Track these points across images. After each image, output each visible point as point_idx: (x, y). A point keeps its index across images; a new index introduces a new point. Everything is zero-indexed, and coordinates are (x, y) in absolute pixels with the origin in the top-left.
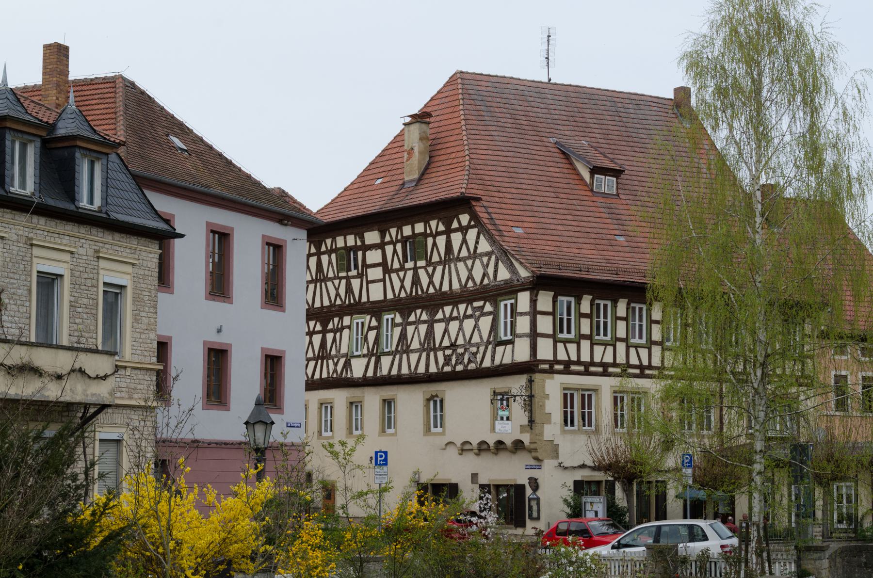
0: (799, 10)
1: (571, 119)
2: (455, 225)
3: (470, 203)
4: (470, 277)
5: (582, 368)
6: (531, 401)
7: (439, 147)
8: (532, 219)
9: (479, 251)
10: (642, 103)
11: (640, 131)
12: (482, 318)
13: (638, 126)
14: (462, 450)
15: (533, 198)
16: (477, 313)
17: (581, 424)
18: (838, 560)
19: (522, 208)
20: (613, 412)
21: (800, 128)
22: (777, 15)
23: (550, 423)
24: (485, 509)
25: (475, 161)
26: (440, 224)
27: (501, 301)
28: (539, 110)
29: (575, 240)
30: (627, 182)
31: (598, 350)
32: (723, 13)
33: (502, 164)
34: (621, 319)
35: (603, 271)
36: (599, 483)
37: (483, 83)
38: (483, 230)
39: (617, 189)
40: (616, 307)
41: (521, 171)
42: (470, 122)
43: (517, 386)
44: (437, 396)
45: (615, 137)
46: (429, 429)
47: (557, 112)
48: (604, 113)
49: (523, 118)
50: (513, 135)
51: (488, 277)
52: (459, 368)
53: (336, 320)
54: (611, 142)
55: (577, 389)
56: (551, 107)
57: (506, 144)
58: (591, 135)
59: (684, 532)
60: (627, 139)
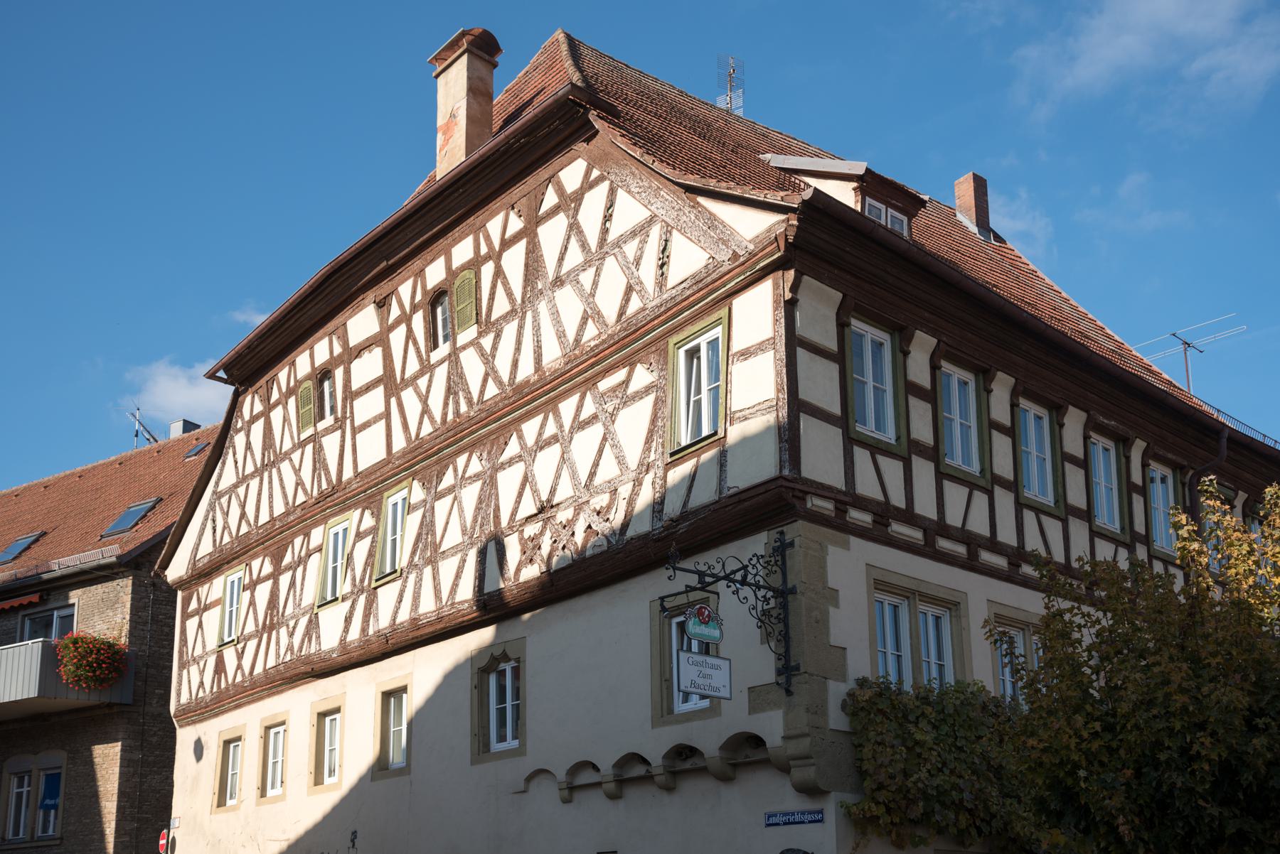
6: (784, 606)
14: (572, 789)
40: (906, 354)
46: (487, 746)
53: (298, 541)
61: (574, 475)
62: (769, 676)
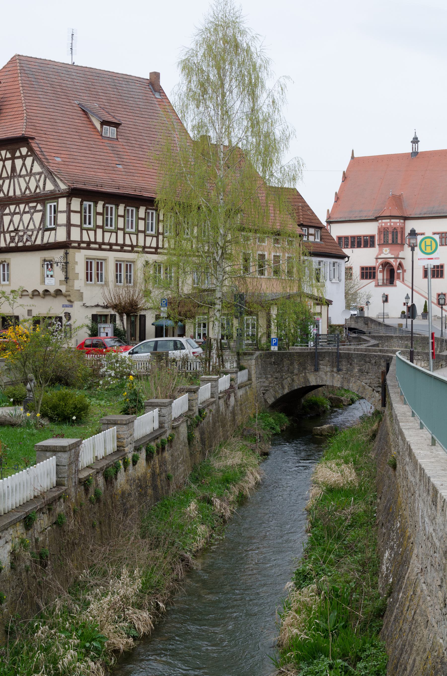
0: (248, 37)
1: (87, 89)
2: (18, 154)
3: (27, 141)
4: (28, 188)
5: (97, 246)
6: (67, 266)
7: (5, 103)
8: (67, 153)
9: (33, 171)
10: (130, 81)
11: (130, 99)
12: (35, 214)
13: (128, 95)
15: (67, 139)
16: (32, 211)
17: (97, 280)
18: (259, 360)
19: (60, 145)
20: (115, 273)
21: (247, 108)
22: (236, 40)
23: (78, 279)
24: (56, 331)
25: (30, 114)
26: (8, 153)
27: (48, 203)
28: (68, 82)
29: (92, 166)
30: (123, 131)
31: (107, 235)
32: (203, 36)
33: (46, 116)
34: (142, 219)
35: (111, 187)
36: (106, 316)
37: (33, 63)
38: (36, 158)
39: (117, 135)
40: (96, 207)
41: (58, 121)
42: (26, 88)
43: (59, 256)
44: (5, 261)
45: (114, 102)
47: (79, 84)
48: (108, 86)
49: (58, 87)
50: (53, 98)
51: (40, 188)
52: (20, 244)
54: (112, 105)
55: (94, 259)
56: (75, 80)
57: (49, 103)
58: (100, 100)
59: (172, 344)
60: (121, 103)
61: (23, 224)
62: (63, 279)
